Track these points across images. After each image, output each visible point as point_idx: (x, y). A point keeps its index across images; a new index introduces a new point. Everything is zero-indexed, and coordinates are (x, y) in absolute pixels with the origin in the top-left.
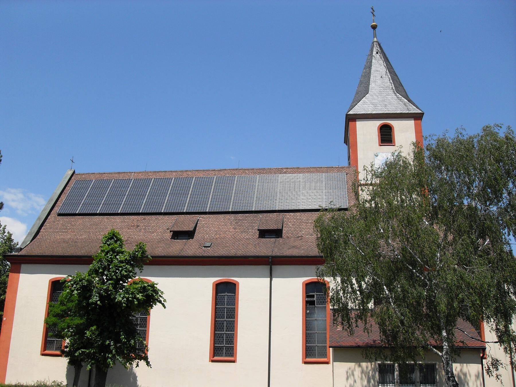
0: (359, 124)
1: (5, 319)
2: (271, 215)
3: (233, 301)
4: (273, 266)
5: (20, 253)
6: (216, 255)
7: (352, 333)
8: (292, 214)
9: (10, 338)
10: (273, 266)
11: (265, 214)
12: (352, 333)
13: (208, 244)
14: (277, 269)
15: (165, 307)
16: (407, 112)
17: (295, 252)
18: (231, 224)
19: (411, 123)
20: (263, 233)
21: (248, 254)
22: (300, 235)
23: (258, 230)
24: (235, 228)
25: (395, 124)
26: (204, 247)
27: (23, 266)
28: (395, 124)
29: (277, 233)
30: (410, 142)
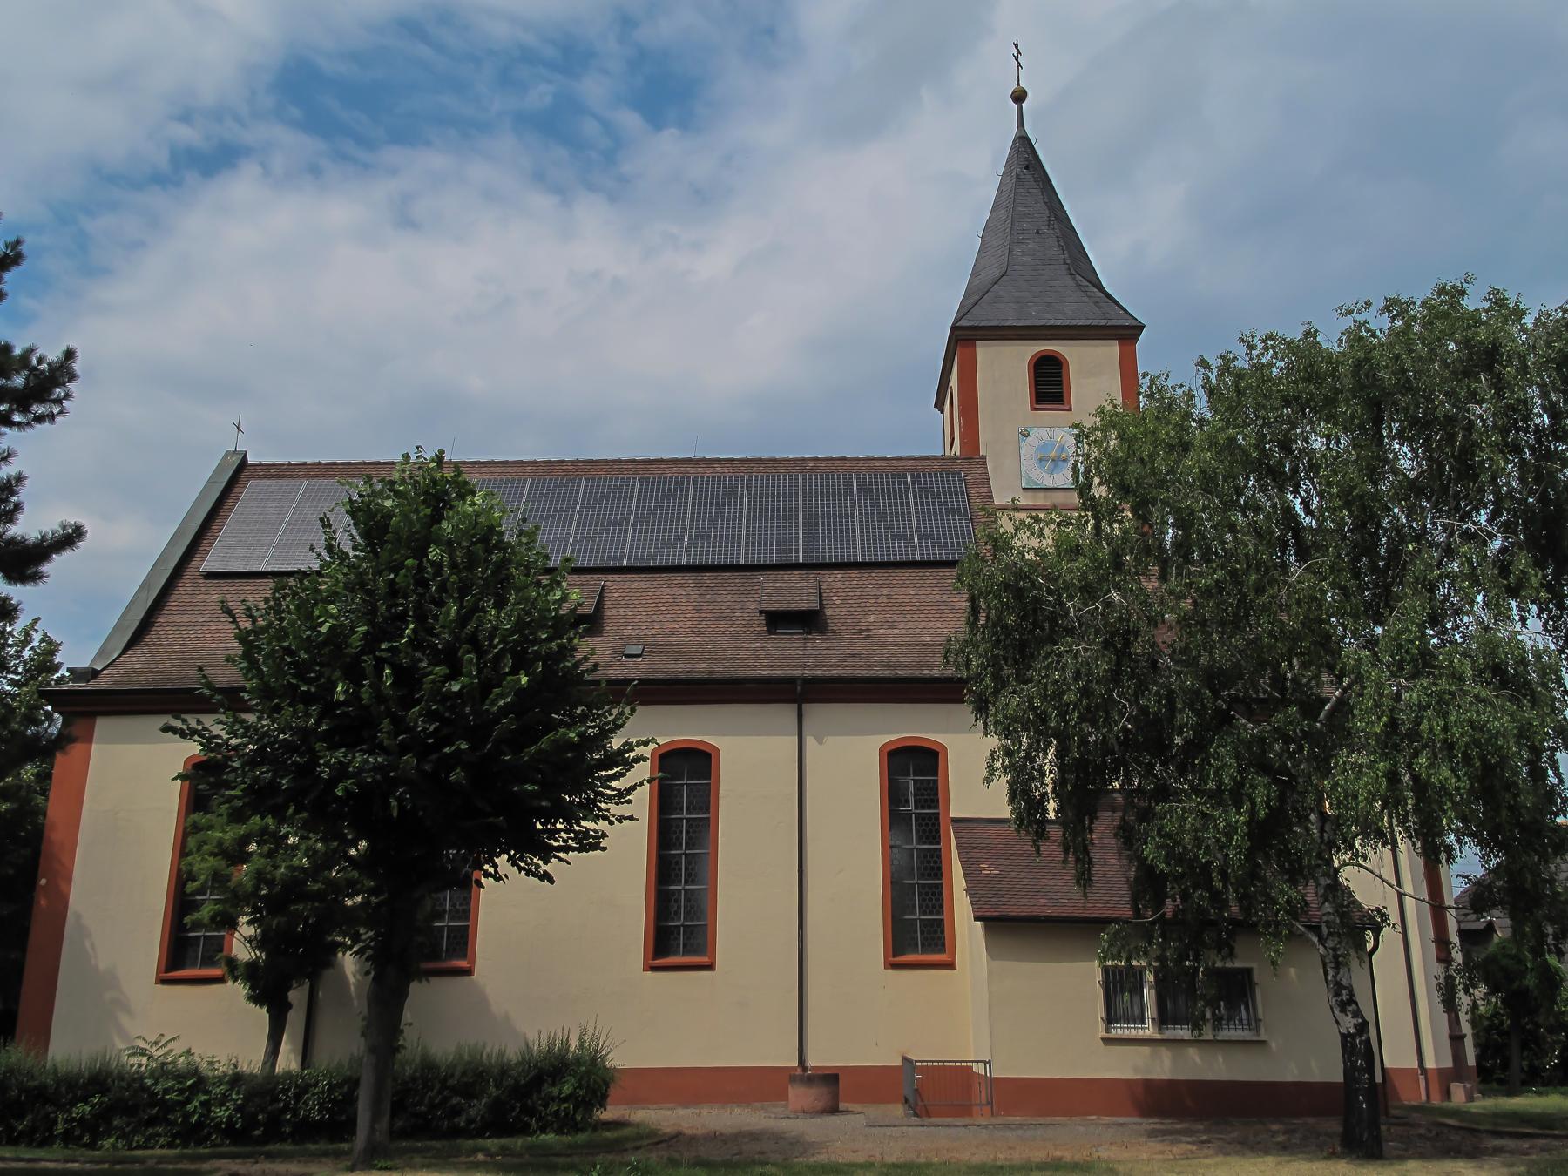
0: (984, 353)
1: (43, 882)
2: (786, 575)
3: (705, 801)
4: (805, 706)
5: (92, 685)
6: (660, 676)
7: (1084, 878)
8: (839, 574)
9: (768, 734)
10: (805, 706)
11: (773, 574)
12: (1084, 878)
13: (636, 650)
14: (817, 713)
15: (551, 881)
16: (1103, 323)
17: (860, 669)
18: (688, 598)
19: (1111, 349)
20: (778, 621)
21: (742, 673)
22: (864, 625)
23: (761, 612)
24: (698, 609)
25: (1072, 352)
26: (627, 656)
27: (102, 725)
28: (1072, 352)
29: (809, 621)
30: (243, 1000)
